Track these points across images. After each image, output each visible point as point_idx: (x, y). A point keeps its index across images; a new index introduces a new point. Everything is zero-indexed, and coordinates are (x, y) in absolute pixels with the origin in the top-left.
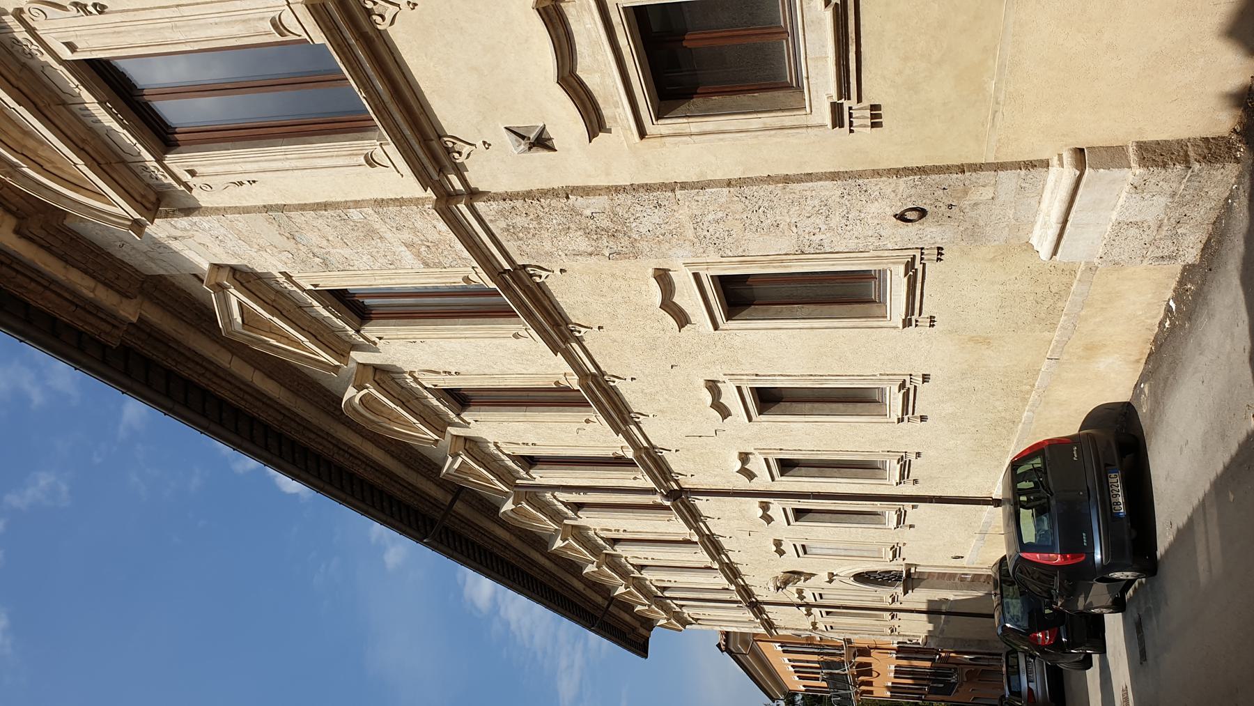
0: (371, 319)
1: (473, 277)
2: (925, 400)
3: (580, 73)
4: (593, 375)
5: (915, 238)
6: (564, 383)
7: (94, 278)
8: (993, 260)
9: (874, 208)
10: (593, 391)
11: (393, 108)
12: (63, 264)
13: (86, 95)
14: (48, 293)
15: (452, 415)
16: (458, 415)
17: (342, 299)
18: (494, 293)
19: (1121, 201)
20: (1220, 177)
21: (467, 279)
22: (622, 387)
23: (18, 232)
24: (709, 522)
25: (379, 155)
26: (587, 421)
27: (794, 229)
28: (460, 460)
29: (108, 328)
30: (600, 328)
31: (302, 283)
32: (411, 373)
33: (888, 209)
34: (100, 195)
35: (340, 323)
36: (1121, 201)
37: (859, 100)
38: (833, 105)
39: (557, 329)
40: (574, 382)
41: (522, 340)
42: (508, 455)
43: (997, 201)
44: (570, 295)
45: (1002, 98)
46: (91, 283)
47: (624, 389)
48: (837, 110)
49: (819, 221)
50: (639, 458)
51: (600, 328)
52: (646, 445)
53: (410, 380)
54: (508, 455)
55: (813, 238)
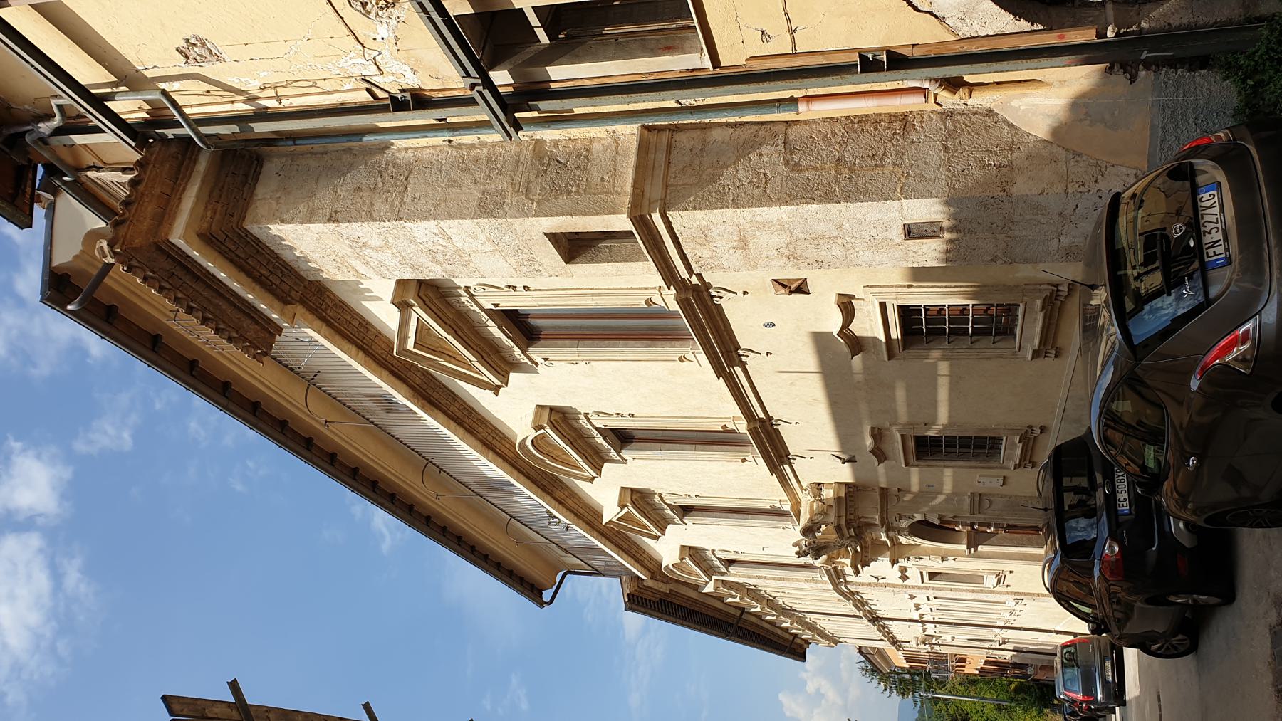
0: (539, 339)
1: (657, 299)
4: (761, 420)
6: (731, 426)
10: (692, 307)
15: (517, 352)
16: (618, 453)
17: (516, 321)
18: (674, 316)
21: (649, 302)
22: (785, 431)
24: (751, 362)
25: (690, 356)
26: (744, 460)
28: (626, 510)
30: (745, 293)
31: (482, 301)
32: (467, 289)
34: (470, 367)
39: (725, 354)
40: (742, 426)
41: (687, 363)
42: (597, 429)
44: (742, 318)
47: (786, 432)
50: (753, 431)
51: (745, 293)
52: (762, 415)
53: (465, 298)
54: (597, 429)
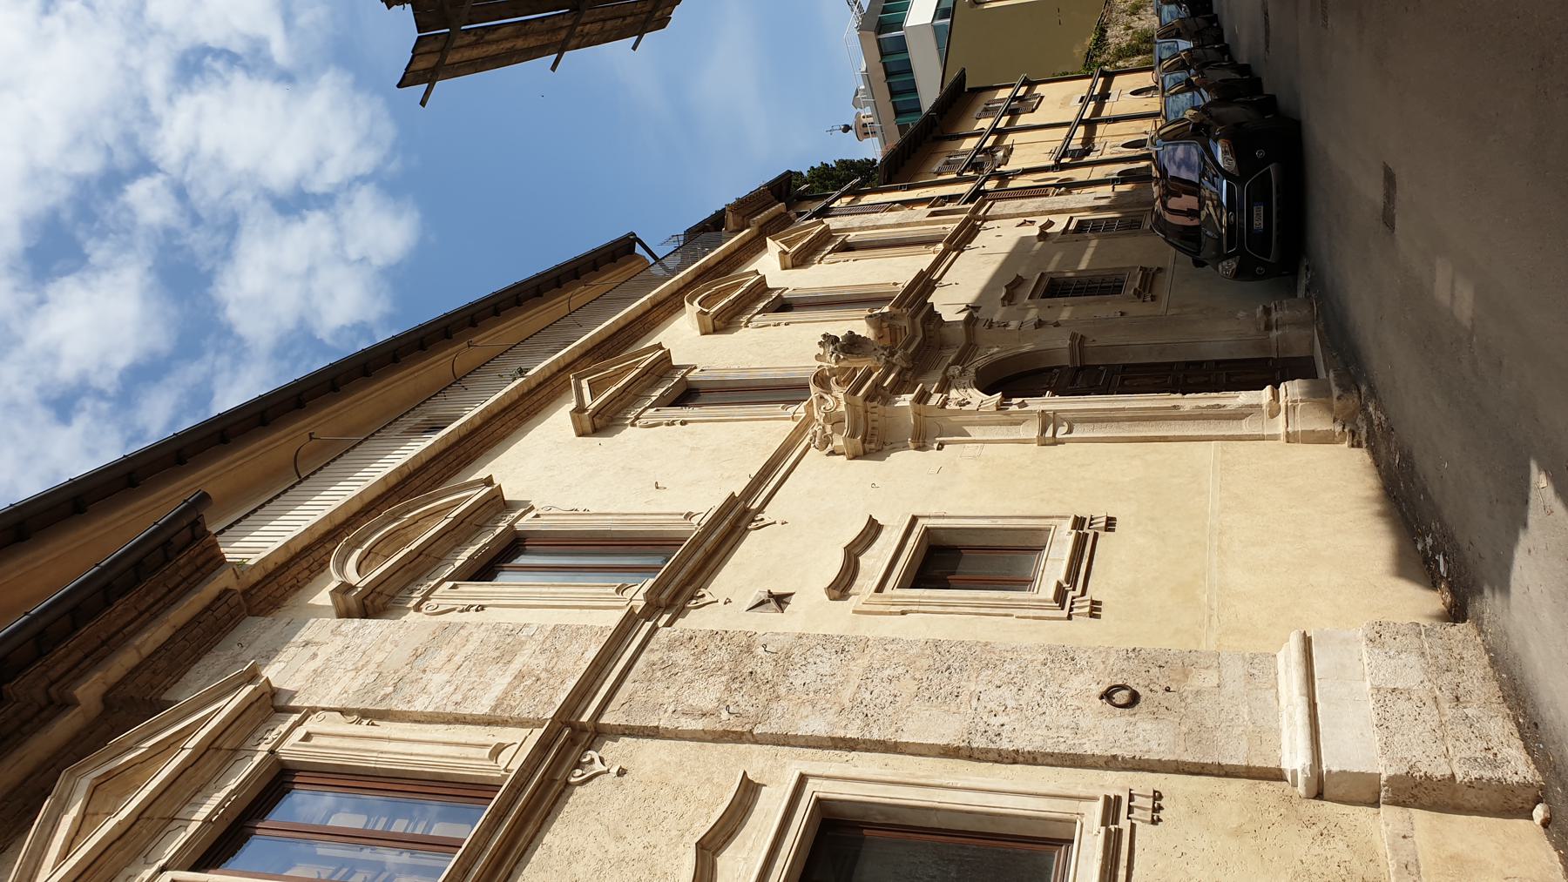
2: (1109, 575)
3: (861, 559)
5: (1123, 738)
7: (150, 656)
8: (1238, 833)
9: (1076, 683)
11: (699, 555)
12: (180, 625)
13: (217, 798)
14: (134, 614)
19: (1366, 660)
20: (1460, 636)
23: (226, 591)
27: (974, 703)
29: (53, 674)
33: (1094, 686)
35: (233, 784)
36: (1366, 660)
37: (1083, 594)
38: (1059, 585)
43: (1223, 692)
45: (1215, 605)
46: (146, 651)
48: (1060, 595)
49: (1007, 693)
55: (993, 720)
